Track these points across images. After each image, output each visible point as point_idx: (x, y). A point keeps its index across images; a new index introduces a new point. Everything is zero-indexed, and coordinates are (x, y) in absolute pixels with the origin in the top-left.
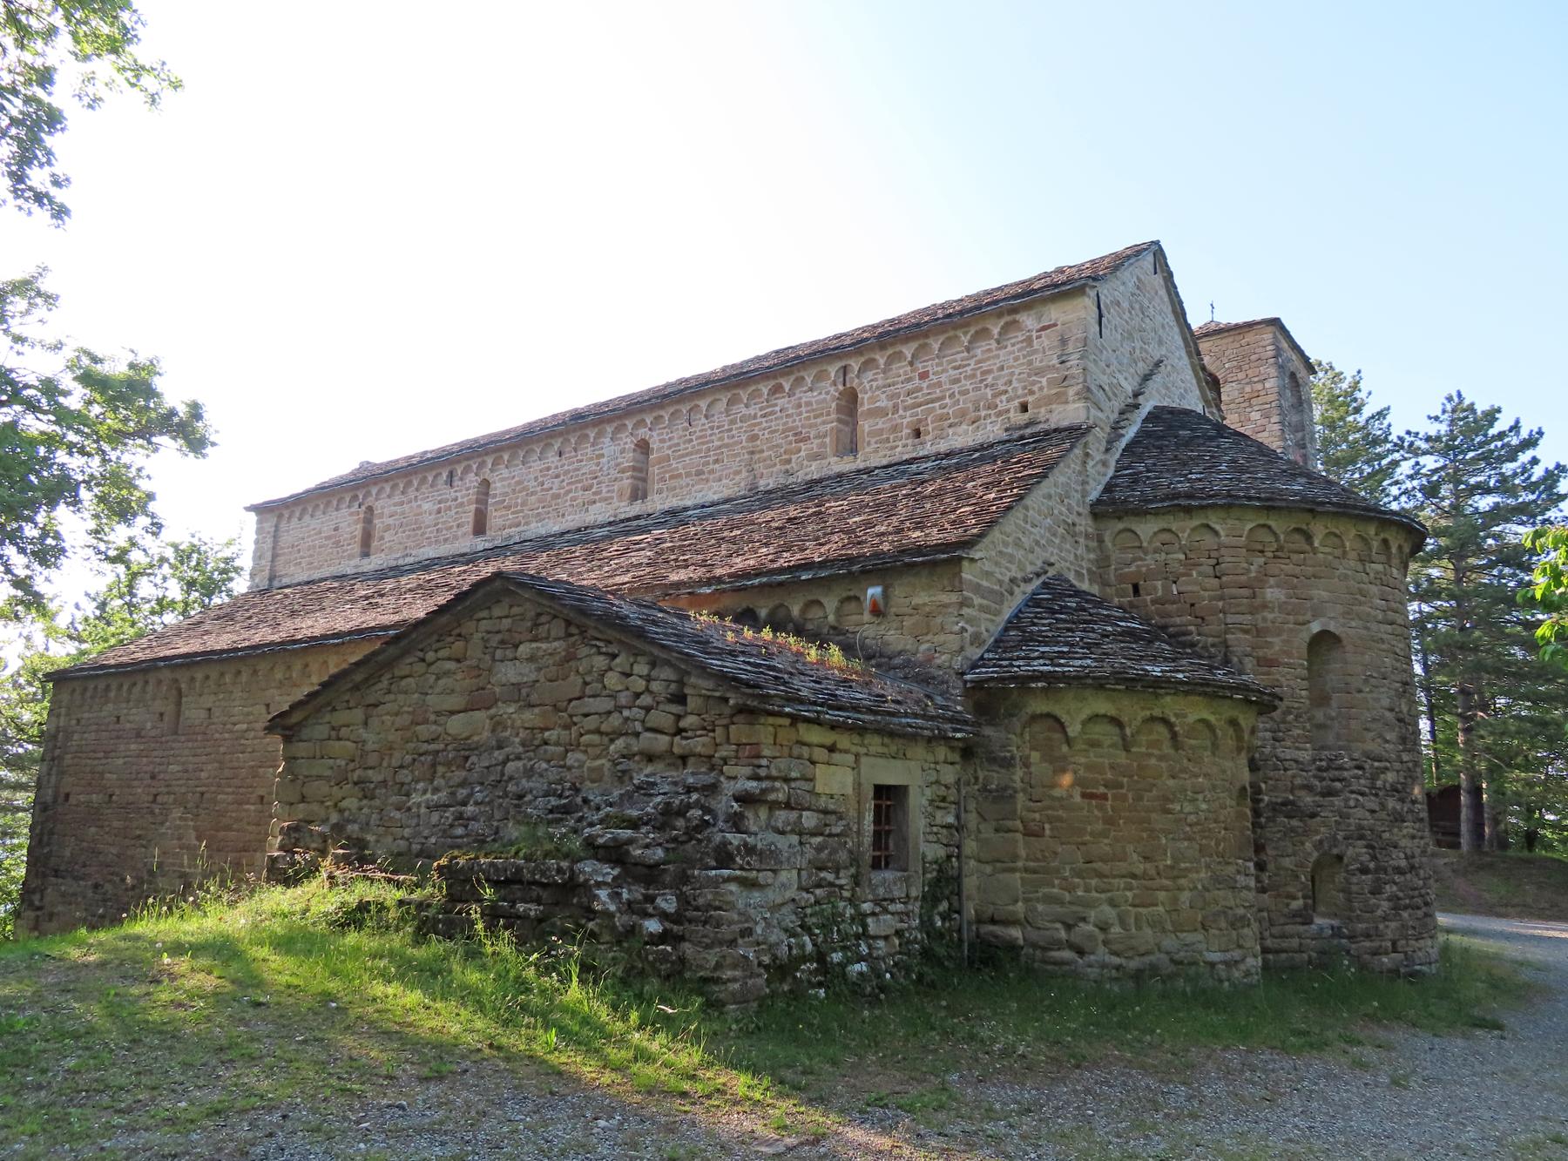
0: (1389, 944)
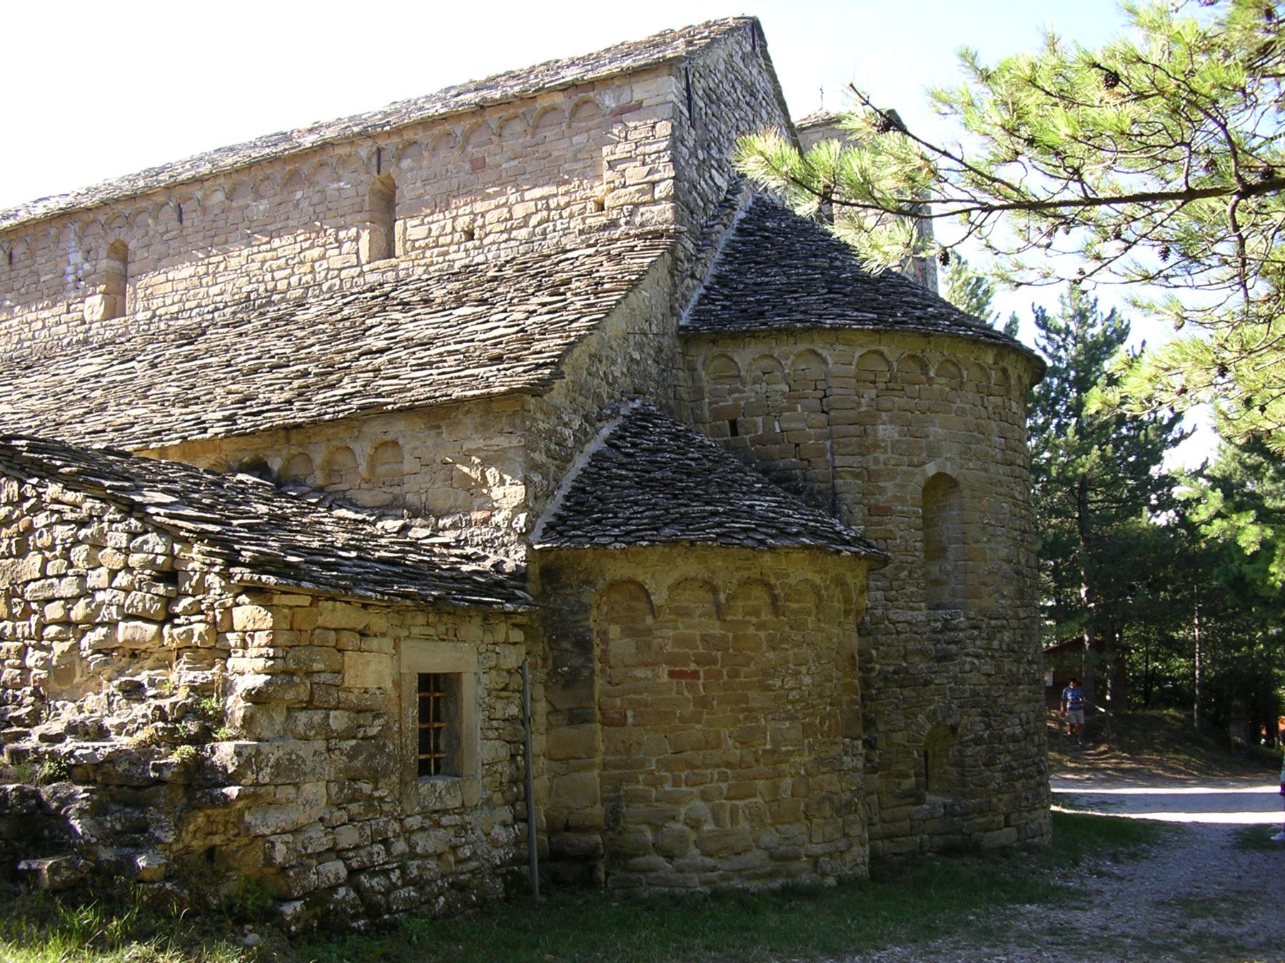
0: (1002, 818)
